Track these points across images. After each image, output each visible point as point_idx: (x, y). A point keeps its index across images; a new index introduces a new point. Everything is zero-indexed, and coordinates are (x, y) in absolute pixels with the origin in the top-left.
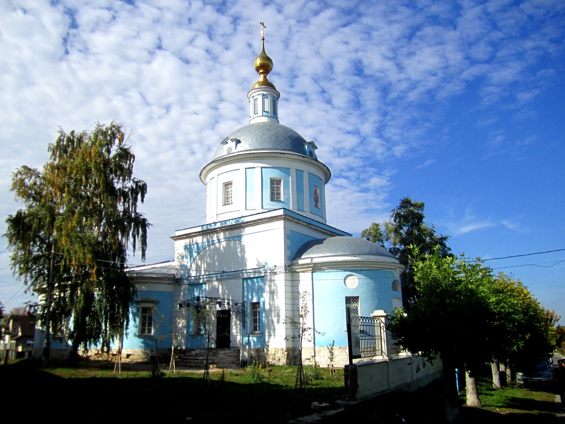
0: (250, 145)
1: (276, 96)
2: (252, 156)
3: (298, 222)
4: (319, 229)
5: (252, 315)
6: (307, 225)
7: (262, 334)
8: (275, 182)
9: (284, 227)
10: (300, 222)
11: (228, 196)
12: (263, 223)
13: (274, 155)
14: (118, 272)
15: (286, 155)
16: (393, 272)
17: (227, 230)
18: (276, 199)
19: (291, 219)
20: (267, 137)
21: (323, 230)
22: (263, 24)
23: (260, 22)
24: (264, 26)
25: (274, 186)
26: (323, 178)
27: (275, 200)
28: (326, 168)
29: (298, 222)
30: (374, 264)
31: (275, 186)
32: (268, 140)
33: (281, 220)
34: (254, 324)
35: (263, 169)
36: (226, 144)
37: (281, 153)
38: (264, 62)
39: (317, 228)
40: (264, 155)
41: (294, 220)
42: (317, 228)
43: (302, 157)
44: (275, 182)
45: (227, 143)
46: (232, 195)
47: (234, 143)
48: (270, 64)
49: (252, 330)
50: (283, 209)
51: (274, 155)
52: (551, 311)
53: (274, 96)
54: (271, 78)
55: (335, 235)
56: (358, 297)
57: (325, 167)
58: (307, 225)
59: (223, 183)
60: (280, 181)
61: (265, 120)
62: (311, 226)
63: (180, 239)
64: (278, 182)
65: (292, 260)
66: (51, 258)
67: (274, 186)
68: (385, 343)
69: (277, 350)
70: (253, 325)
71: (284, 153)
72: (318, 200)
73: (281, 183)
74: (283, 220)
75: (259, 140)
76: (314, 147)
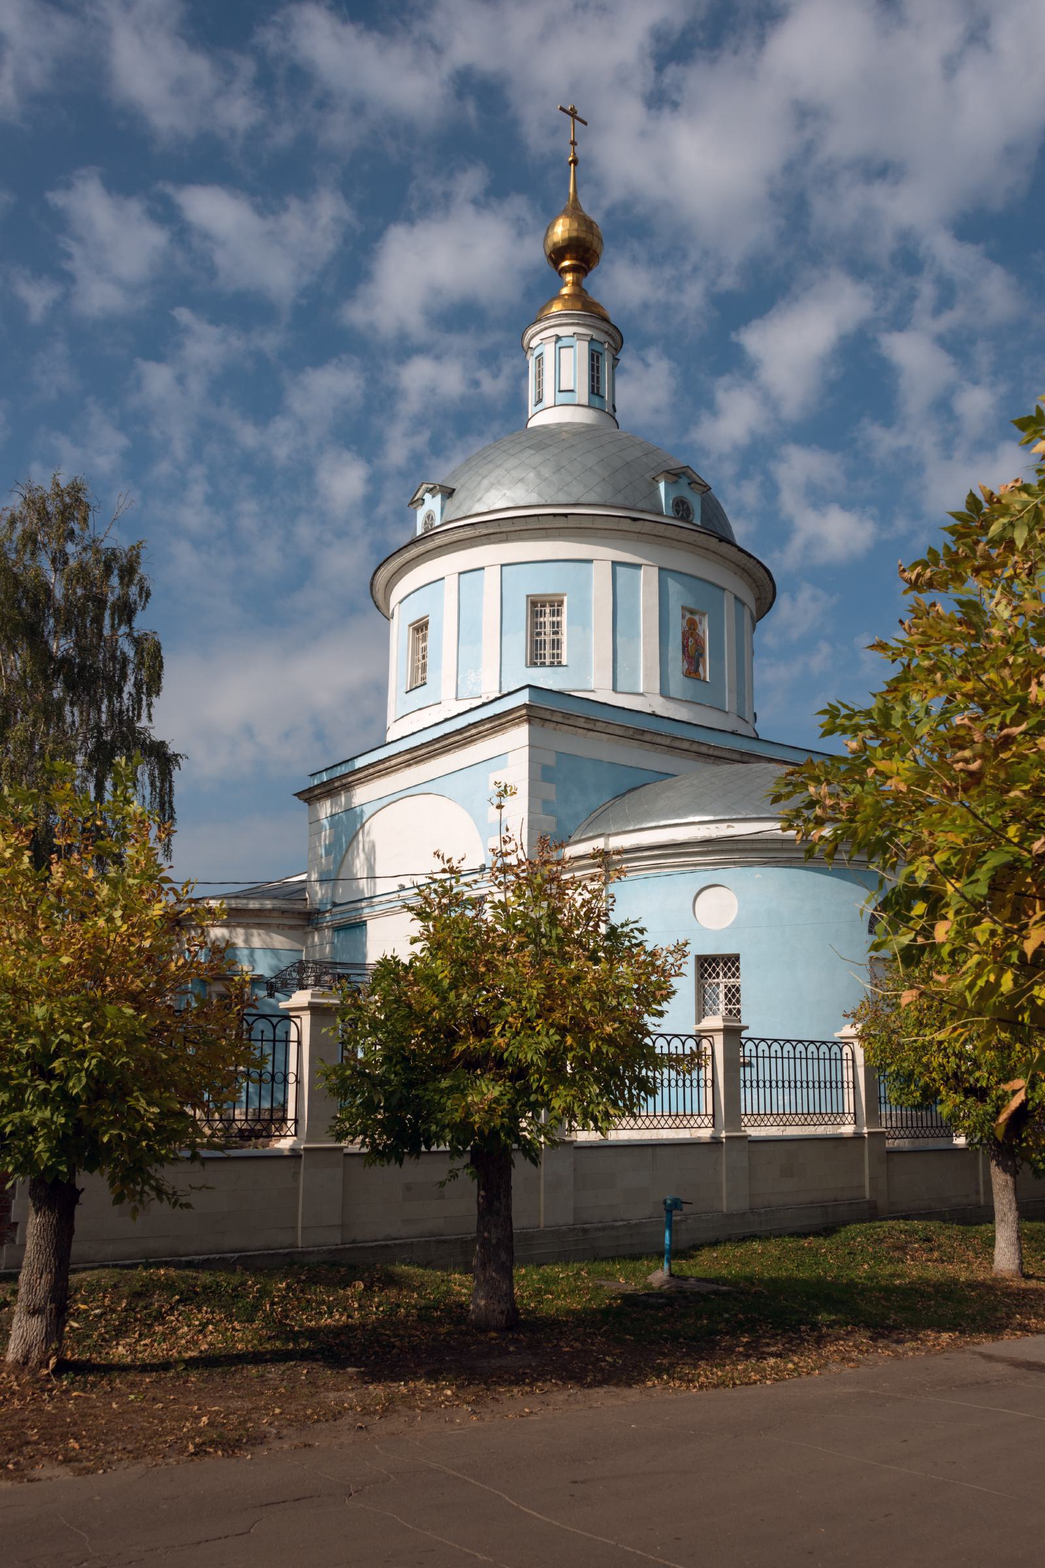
0: (539, 494)
4: (686, 745)
9: (530, 746)
22: (573, 113)
25: (546, 619)
33: (522, 722)
35: (619, 569)
36: (422, 505)
37: (555, 515)
38: (583, 235)
39: (659, 740)
42: (676, 744)
43: (629, 521)
46: (428, 660)
48: (595, 243)
50: (527, 691)
52: (386, 1167)
53: (592, 339)
55: (752, 759)
59: (410, 626)
61: (582, 417)
64: (556, 605)
67: (546, 619)
68: (807, 1117)
71: (566, 515)
72: (702, 654)
74: (525, 720)
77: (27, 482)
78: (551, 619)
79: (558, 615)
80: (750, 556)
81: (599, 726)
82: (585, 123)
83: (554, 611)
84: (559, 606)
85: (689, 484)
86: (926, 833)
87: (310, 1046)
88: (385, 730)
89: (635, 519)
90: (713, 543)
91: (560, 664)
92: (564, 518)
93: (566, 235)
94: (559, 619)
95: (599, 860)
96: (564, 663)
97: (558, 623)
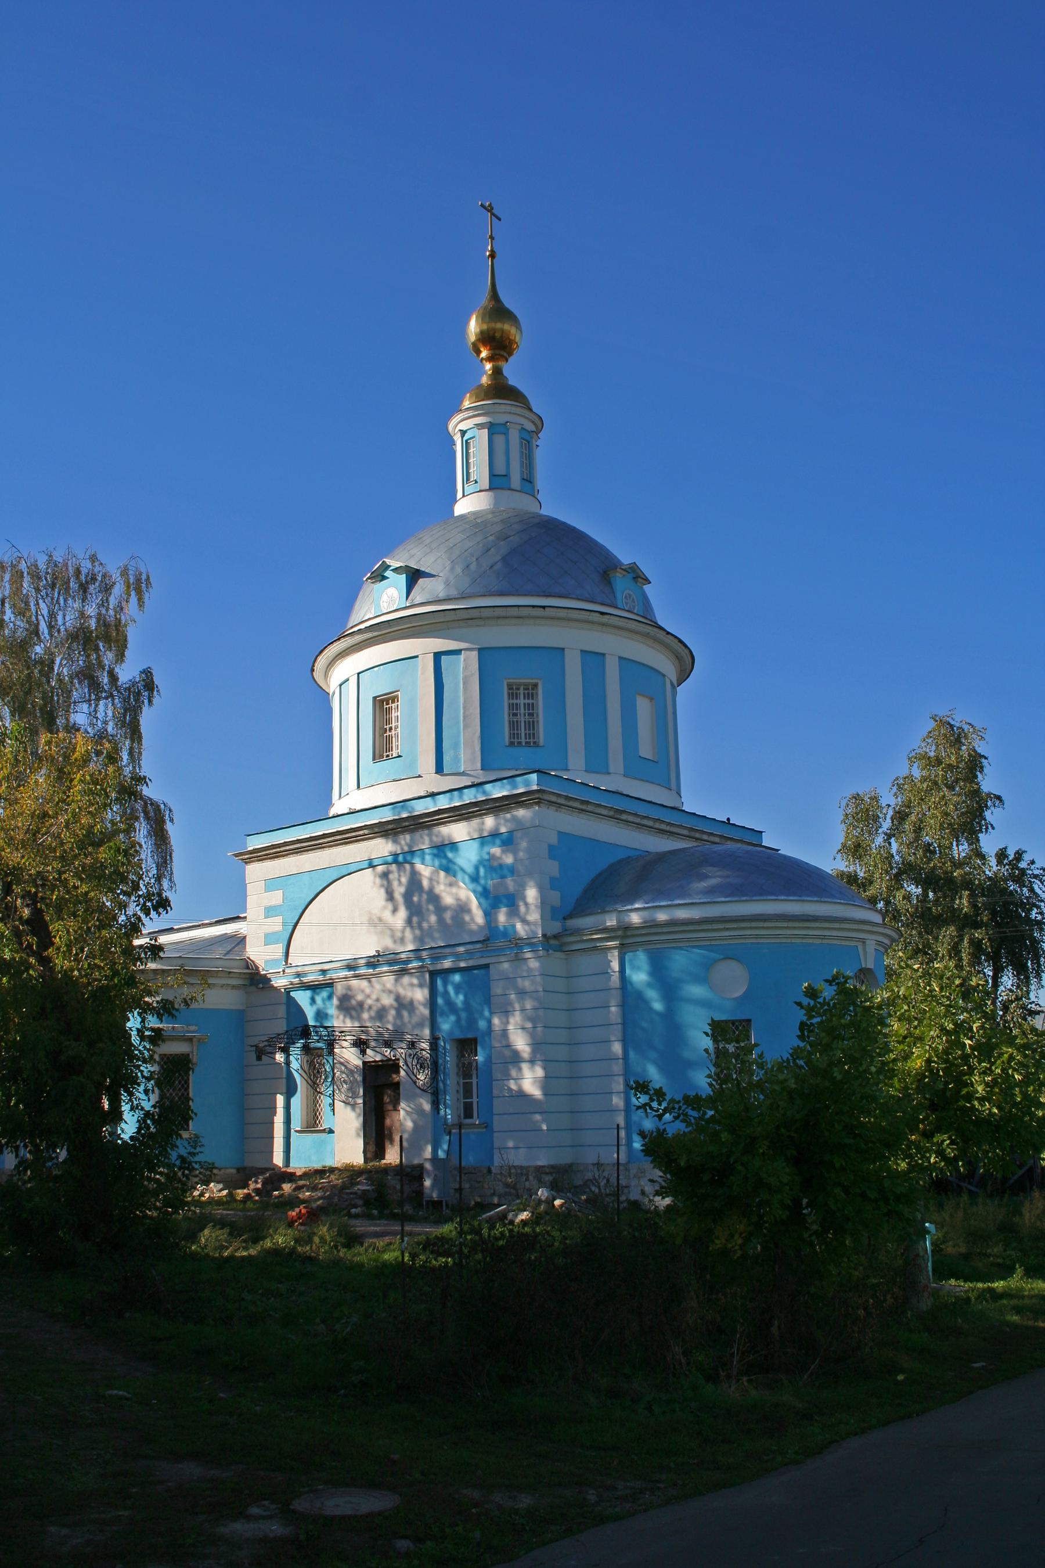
1: (530, 427)
2: (451, 616)
3: (584, 807)
4: (650, 823)
5: (457, 1074)
6: (611, 813)
7: (486, 1127)
8: (522, 691)
10: (590, 808)
11: (388, 733)
12: (321, 847)
13: (514, 612)
14: (902, 1145)
15: (548, 612)
16: (857, 946)
17: (406, 830)
18: (523, 740)
19: (561, 801)
20: (498, 558)
21: (663, 827)
22: (490, 209)
23: (482, 205)
24: (493, 214)
26: (668, 668)
27: (520, 743)
28: (676, 641)
29: (584, 807)
30: (795, 928)
31: (522, 701)
32: (499, 566)
34: (464, 1098)
36: (381, 581)
37: (533, 607)
39: (645, 822)
40: (486, 613)
41: (571, 803)
42: (645, 822)
43: (597, 615)
44: (522, 691)
45: (384, 578)
47: (403, 578)
49: (459, 1117)
51: (514, 612)
54: (513, 372)
56: (749, 1021)
57: (670, 637)
58: (611, 813)
60: (535, 686)
62: (624, 817)
63: (261, 859)
64: (531, 691)
65: (565, 919)
66: (955, 1024)
69: (525, 1171)
70: (463, 1101)
71: (544, 607)
73: (537, 694)
75: (473, 567)
76: (640, 580)
77: (52, 550)
78: (518, 701)
79: (517, 699)
80: (685, 646)
81: (590, 808)
82: (500, 220)
83: (513, 693)
84: (533, 689)
85: (634, 578)
86: (408, 1477)
87: (272, 1152)
88: (330, 804)
89: (603, 614)
90: (649, 629)
91: (536, 745)
92: (542, 609)
93: (478, 330)
94: (511, 701)
95: (620, 933)
96: (541, 743)
97: (517, 704)
